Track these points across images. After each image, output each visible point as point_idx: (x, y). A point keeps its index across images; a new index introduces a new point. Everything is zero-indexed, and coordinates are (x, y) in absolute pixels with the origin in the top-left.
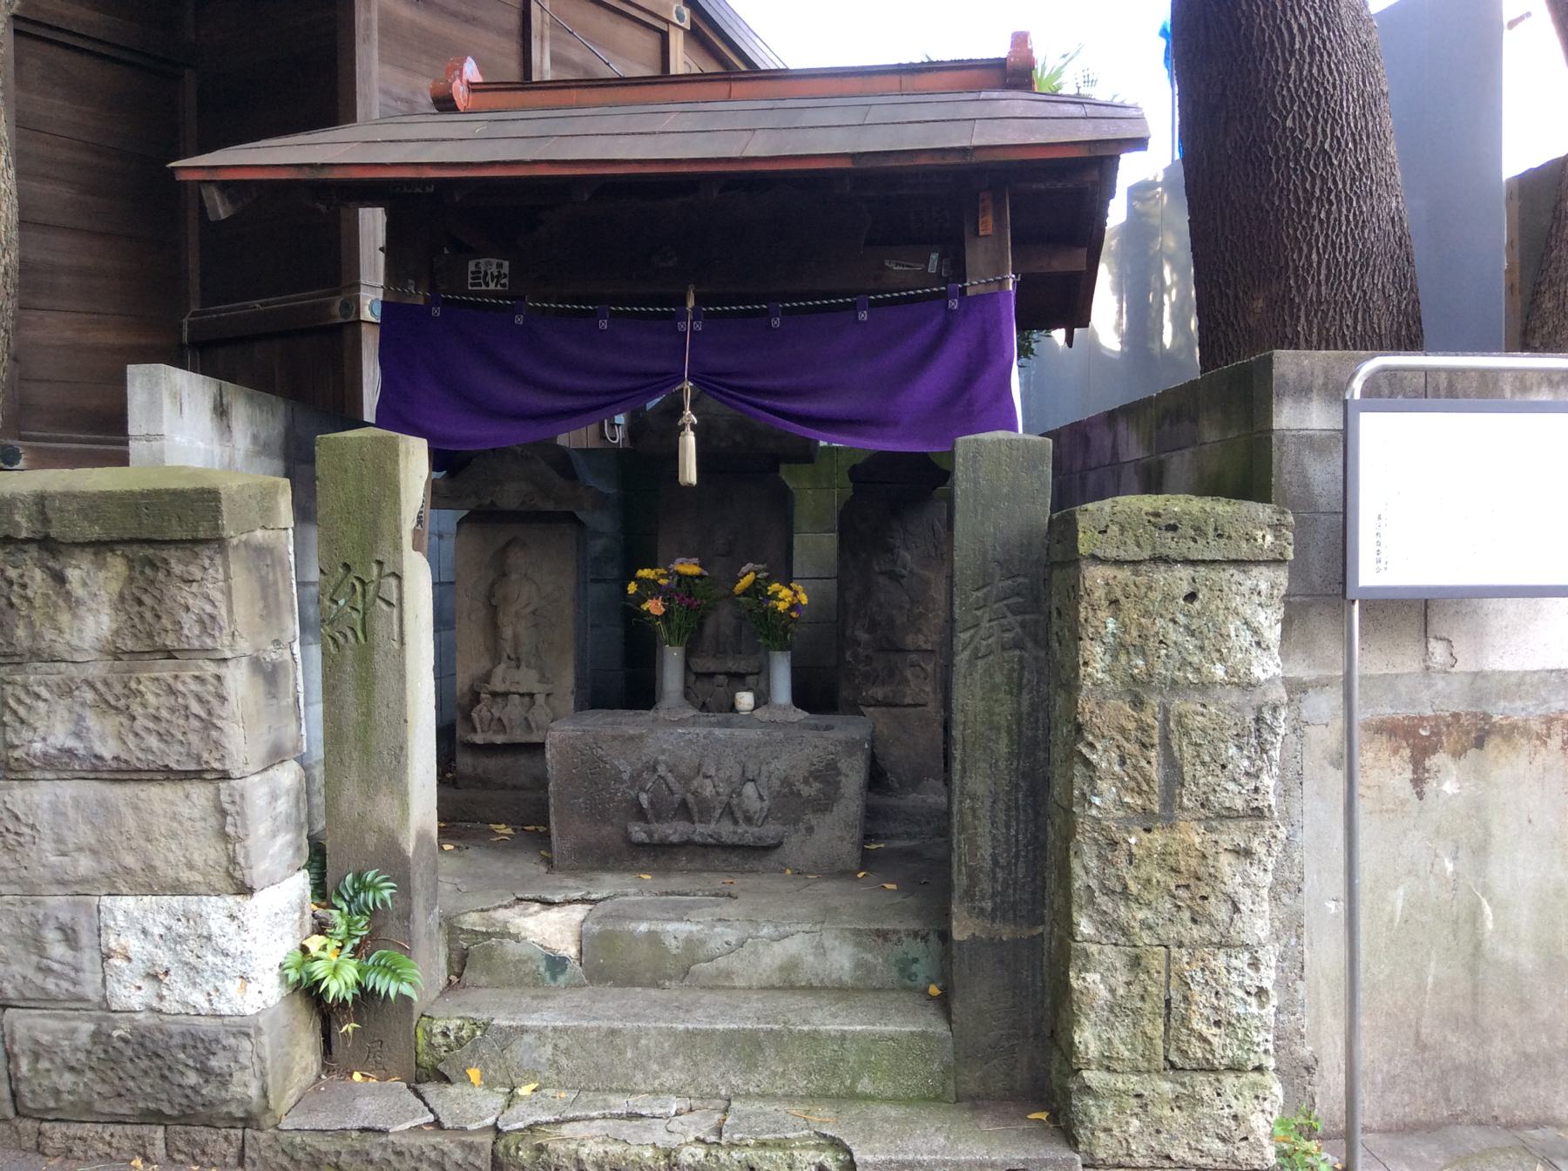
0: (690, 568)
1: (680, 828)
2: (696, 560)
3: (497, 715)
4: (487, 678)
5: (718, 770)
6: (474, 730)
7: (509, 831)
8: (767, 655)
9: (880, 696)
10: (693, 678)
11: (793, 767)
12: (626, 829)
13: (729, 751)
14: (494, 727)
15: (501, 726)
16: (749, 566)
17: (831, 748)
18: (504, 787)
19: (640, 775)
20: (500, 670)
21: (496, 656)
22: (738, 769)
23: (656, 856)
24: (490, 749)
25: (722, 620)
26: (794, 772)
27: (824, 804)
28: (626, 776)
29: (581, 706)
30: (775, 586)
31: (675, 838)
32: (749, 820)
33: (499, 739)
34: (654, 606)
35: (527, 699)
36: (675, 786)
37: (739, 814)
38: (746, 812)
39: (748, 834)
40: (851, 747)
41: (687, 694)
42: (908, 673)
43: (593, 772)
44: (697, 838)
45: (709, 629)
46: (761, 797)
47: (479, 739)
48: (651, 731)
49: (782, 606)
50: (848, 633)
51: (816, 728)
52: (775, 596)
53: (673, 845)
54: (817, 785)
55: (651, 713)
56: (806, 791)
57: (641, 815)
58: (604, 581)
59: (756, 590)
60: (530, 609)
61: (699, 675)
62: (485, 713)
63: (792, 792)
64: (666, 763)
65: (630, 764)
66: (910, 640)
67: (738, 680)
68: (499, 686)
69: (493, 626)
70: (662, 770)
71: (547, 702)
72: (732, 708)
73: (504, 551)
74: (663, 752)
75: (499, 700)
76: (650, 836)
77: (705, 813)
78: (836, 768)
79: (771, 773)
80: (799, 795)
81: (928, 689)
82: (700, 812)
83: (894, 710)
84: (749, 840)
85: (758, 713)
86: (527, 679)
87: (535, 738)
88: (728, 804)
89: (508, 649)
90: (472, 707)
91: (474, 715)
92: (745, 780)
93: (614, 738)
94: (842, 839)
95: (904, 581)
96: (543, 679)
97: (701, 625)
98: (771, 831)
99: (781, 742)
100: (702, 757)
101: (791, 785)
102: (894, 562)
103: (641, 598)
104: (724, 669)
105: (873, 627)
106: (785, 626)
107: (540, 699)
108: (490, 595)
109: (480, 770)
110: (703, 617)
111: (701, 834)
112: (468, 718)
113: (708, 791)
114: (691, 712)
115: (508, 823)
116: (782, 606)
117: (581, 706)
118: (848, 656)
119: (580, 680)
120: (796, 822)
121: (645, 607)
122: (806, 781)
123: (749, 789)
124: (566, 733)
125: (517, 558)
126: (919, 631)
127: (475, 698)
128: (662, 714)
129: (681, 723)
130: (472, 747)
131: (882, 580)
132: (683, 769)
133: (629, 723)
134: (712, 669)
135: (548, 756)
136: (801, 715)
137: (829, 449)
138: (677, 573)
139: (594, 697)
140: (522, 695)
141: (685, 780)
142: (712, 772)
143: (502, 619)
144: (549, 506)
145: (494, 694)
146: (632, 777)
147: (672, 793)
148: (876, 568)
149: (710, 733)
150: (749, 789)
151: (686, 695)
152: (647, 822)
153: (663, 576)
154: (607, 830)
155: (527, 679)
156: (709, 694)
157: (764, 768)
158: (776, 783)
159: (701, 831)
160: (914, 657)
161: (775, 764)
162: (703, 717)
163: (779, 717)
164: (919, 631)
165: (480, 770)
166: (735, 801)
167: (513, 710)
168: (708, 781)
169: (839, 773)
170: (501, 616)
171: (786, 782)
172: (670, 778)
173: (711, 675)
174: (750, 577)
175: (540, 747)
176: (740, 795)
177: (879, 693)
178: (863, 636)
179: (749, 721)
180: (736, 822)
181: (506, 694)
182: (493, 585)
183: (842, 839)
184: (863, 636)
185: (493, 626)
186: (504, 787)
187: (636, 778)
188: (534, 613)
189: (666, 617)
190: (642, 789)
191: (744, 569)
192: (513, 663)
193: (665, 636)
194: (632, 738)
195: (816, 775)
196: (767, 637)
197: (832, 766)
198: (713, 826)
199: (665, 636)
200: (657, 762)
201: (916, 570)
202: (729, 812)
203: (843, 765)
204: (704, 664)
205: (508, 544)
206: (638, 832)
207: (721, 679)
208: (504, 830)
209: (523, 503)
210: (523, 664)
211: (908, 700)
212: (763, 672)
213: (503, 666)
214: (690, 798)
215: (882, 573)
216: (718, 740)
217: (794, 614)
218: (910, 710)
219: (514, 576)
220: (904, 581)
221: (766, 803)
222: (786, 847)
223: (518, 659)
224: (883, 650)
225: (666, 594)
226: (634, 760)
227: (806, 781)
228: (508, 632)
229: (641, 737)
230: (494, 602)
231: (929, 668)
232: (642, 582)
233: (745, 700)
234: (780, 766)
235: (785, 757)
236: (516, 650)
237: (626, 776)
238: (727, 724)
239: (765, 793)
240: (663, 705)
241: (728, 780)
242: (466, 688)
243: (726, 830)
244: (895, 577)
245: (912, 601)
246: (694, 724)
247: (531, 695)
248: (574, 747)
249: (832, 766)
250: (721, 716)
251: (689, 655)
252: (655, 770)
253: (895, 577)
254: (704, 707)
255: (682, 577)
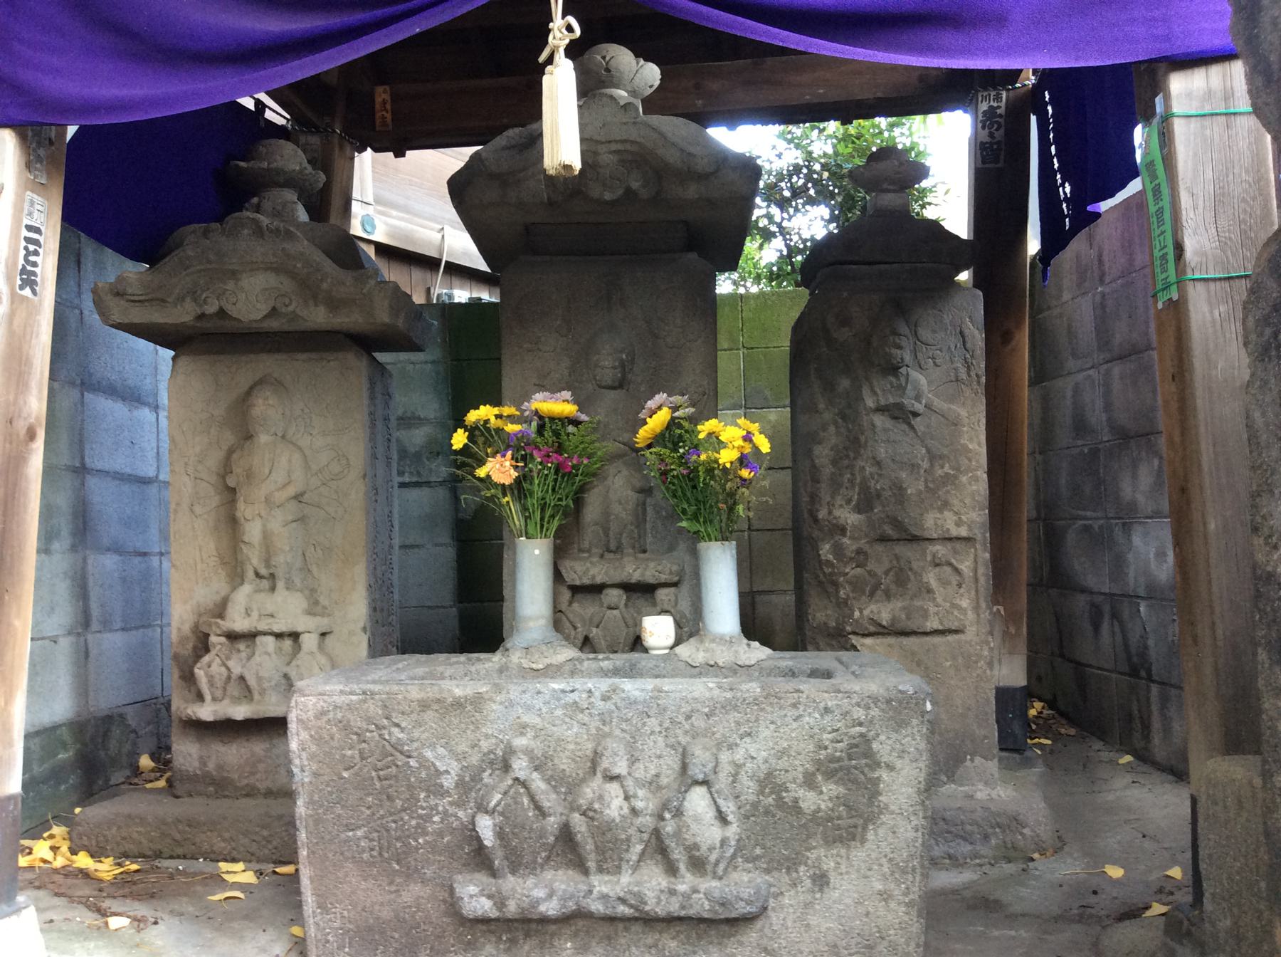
0: (558, 405)
1: (560, 886)
2: (567, 394)
3: (237, 670)
4: (220, 610)
5: (633, 761)
6: (200, 697)
7: (249, 877)
8: (695, 554)
9: (885, 618)
10: (566, 595)
11: (783, 753)
12: (452, 890)
13: (653, 723)
14: (234, 690)
15: (246, 690)
16: (660, 397)
17: (859, 713)
18: (251, 793)
19: (477, 778)
20: (242, 595)
21: (236, 576)
22: (670, 764)
23: (513, 941)
24: (226, 729)
25: (615, 493)
26: (783, 764)
27: (848, 827)
28: (448, 782)
29: (377, 650)
30: (710, 425)
31: (550, 908)
32: (698, 864)
33: (240, 712)
34: (500, 469)
35: (288, 643)
36: (549, 800)
37: (678, 854)
38: (692, 848)
39: (698, 891)
40: (898, 710)
41: (558, 620)
42: (931, 578)
43: (383, 775)
44: (597, 907)
45: (592, 511)
46: (722, 818)
47: (206, 712)
48: (498, 688)
49: (727, 457)
50: (822, 514)
51: (792, 674)
52: (715, 442)
53: (544, 920)
54: (831, 789)
55: (497, 658)
56: (809, 801)
57: (479, 858)
58: (428, 484)
59: (673, 435)
60: (291, 491)
61: (576, 590)
62: (217, 669)
63: (780, 803)
64: (528, 752)
65: (461, 757)
66: (932, 522)
67: (643, 593)
68: (239, 623)
69: (230, 523)
70: (520, 766)
71: (321, 647)
72: (637, 643)
73: (245, 399)
74: (522, 729)
75: (242, 646)
76: (500, 903)
77: (610, 851)
78: (869, 754)
79: (738, 766)
80: (796, 807)
81: (965, 603)
82: (600, 850)
83: (906, 641)
84: (701, 906)
85: (682, 650)
86: (288, 609)
87: (271, 708)
88: (656, 833)
89: (254, 559)
90: (198, 657)
91: (199, 672)
92: (687, 779)
93: (424, 705)
94: (885, 896)
95: (917, 422)
96: (314, 608)
97: (579, 502)
98: (742, 884)
99: (756, 701)
100: (600, 737)
101: (779, 789)
102: (902, 389)
103: (471, 458)
104: (618, 576)
105: (865, 504)
106: (732, 494)
107: (309, 641)
108: (226, 468)
109: (211, 766)
110: (582, 489)
111: (604, 897)
112: (189, 678)
113: (615, 807)
114: (566, 653)
115: (248, 858)
116: (727, 457)
117: (377, 650)
118: (826, 551)
119: (376, 609)
120: (791, 864)
121: (481, 472)
122: (809, 782)
123: (698, 801)
124: (334, 694)
125: (266, 407)
126: (946, 505)
127: (202, 645)
128: (516, 658)
129: (551, 671)
130: (199, 727)
131: (880, 421)
132: (564, 763)
133: (458, 676)
134: (599, 580)
135: (294, 745)
136: (758, 653)
137: (733, 297)
138: (536, 412)
139: (404, 635)
140: (279, 636)
141: (567, 786)
142: (621, 768)
143: (243, 510)
144: (318, 317)
145: (233, 637)
146: (460, 783)
147: (541, 812)
148: (870, 403)
149: (614, 690)
150: (698, 801)
151: (557, 625)
152: (494, 873)
153: (512, 419)
154: (413, 892)
155: (288, 609)
156: (599, 620)
157: (724, 757)
158: (749, 787)
159: (604, 889)
160: (940, 550)
161: (747, 747)
162: (589, 662)
163: (723, 656)
164: (946, 505)
165: (211, 766)
166: (669, 827)
167: (265, 661)
168: (614, 788)
169: (876, 765)
170: (241, 505)
171: (768, 782)
172: (538, 784)
173: (595, 589)
174: (663, 416)
175: (276, 726)
176: (678, 813)
177: (884, 612)
178: (850, 518)
179: (670, 666)
180: (672, 870)
181: (251, 636)
182: (230, 452)
183: (885, 896)
184: (850, 518)
185: (230, 523)
186: (251, 793)
187: (469, 785)
188: (298, 497)
189: (519, 488)
190: (482, 808)
191: (651, 404)
192: (265, 584)
193: (517, 520)
194: (458, 704)
195: (829, 768)
196: (695, 517)
197: (861, 749)
198: (625, 878)
199: (517, 520)
200: (510, 751)
201: (938, 403)
202: (658, 848)
203: (883, 747)
204: (584, 570)
205: (261, 382)
206: (475, 897)
207: (614, 595)
208: (239, 873)
209: (274, 312)
210: (280, 585)
211: (933, 624)
212: (689, 582)
213: (246, 589)
214: (577, 820)
215: (880, 409)
216: (632, 703)
217: (745, 473)
218: (937, 640)
219: (263, 438)
220: (917, 422)
221: (733, 831)
222: (775, 918)
223: (272, 576)
224: (883, 539)
225: (521, 450)
226: (463, 747)
227: (809, 782)
228: (253, 532)
229: (477, 701)
230: (231, 482)
231: (966, 566)
232: (473, 431)
233: (658, 629)
234: (756, 751)
235: (766, 732)
236: (268, 563)
237: (448, 782)
238: (631, 672)
239: (729, 807)
240: (516, 642)
241: (653, 784)
242: (187, 628)
243: (651, 886)
244: (900, 414)
245: (933, 457)
246: (573, 673)
247: (295, 636)
248: (345, 727)
249: (861, 749)
250: (620, 659)
251: (559, 553)
252: (507, 767)
253: (900, 414)
254: (587, 644)
255: (544, 422)
